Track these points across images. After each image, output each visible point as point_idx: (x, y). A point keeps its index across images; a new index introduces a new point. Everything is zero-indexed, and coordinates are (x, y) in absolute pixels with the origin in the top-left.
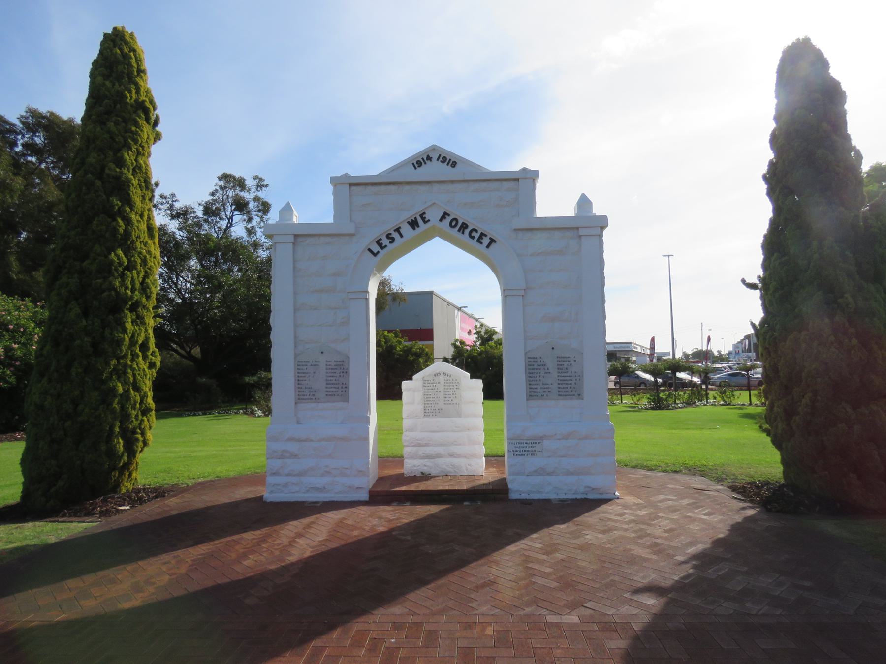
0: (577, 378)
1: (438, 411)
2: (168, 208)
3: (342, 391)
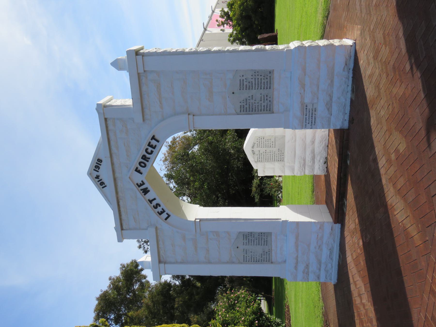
0: (256, 75)
1: (280, 152)
2: (147, 244)
3: (264, 236)
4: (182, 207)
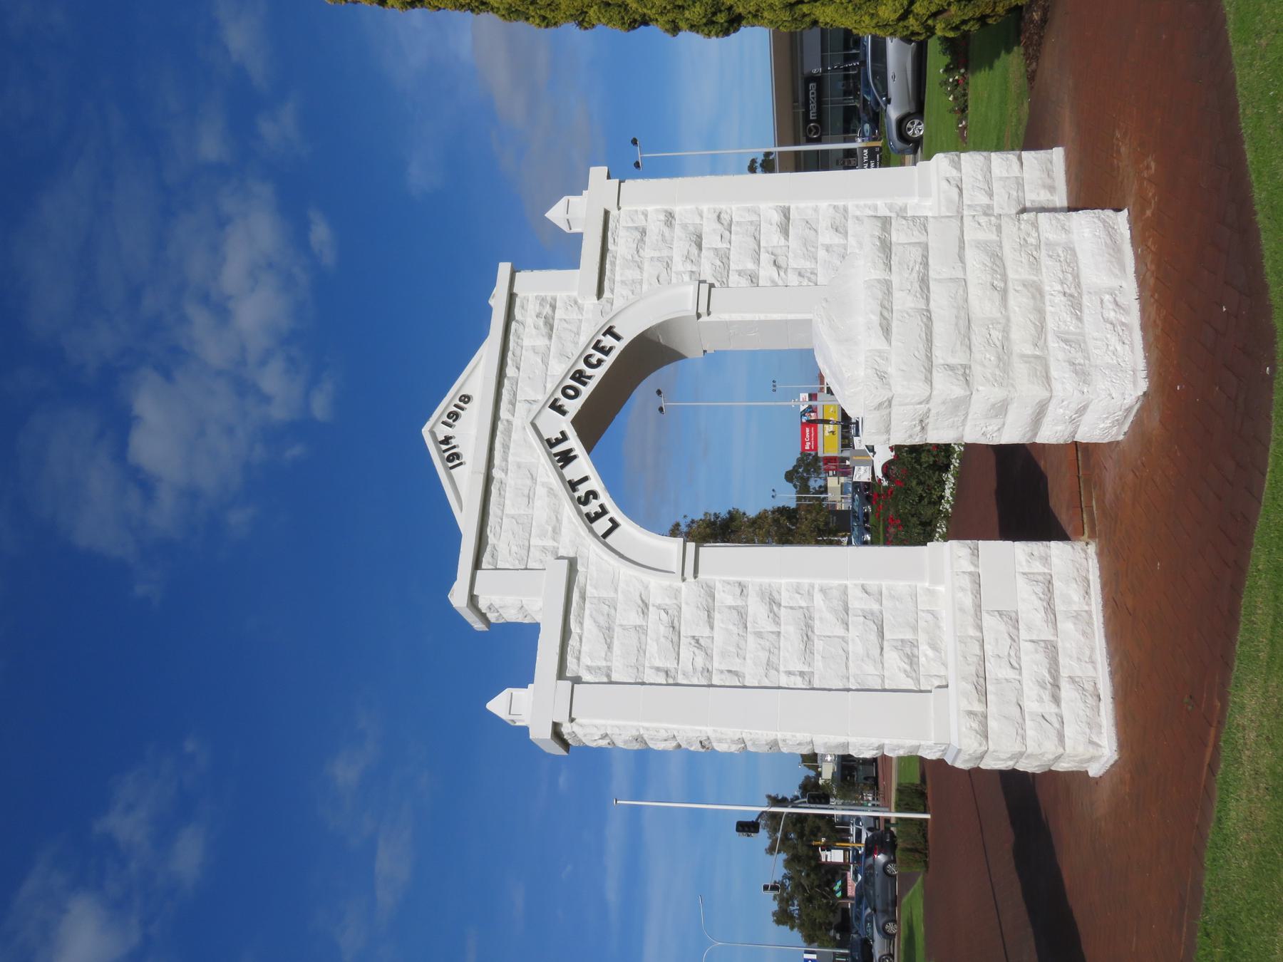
4: (659, 340)
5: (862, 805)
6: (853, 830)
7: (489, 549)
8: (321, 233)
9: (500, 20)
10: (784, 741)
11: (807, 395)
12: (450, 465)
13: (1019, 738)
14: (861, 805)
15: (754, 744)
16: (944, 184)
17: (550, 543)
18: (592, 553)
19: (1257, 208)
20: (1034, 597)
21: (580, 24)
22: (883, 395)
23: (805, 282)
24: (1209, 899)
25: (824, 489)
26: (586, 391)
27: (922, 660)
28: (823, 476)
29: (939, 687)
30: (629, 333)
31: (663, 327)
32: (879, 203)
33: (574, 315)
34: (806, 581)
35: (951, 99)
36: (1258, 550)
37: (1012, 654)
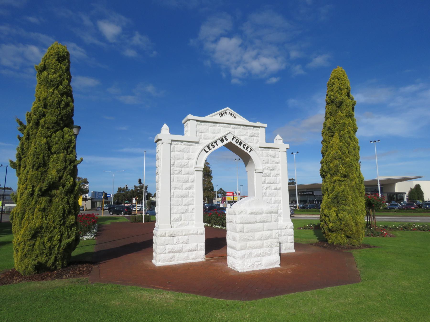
5: (146, 207)
6: (140, 205)
7: (201, 123)
8: (274, 80)
9: (323, 123)
10: (159, 191)
11: (240, 193)
12: (220, 114)
13: (160, 244)
14: (146, 207)
15: (158, 185)
16: (286, 225)
17: (202, 137)
18: (200, 147)
19: (279, 296)
20: (192, 247)
21: (323, 141)
22: (237, 213)
23: (263, 194)
24: (125, 287)
25: (218, 197)
26: (237, 145)
27: (178, 222)
28: (221, 197)
29: (171, 226)
30: (251, 154)
31: (252, 162)
32: (282, 211)
33: (255, 141)
34: (195, 196)
35: (307, 225)
36: (202, 297)
37: (179, 242)
